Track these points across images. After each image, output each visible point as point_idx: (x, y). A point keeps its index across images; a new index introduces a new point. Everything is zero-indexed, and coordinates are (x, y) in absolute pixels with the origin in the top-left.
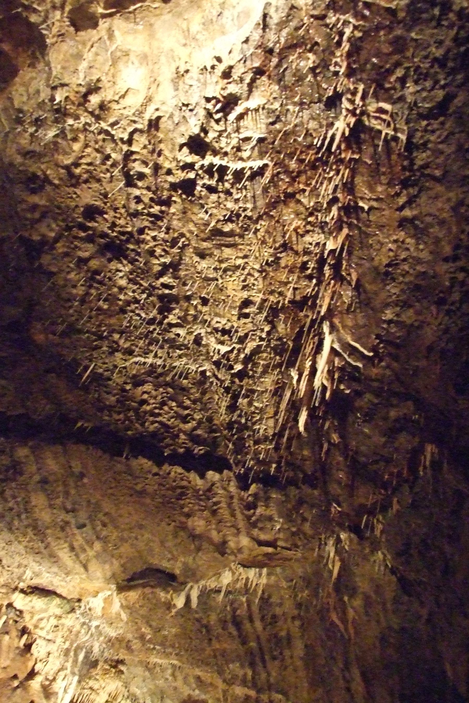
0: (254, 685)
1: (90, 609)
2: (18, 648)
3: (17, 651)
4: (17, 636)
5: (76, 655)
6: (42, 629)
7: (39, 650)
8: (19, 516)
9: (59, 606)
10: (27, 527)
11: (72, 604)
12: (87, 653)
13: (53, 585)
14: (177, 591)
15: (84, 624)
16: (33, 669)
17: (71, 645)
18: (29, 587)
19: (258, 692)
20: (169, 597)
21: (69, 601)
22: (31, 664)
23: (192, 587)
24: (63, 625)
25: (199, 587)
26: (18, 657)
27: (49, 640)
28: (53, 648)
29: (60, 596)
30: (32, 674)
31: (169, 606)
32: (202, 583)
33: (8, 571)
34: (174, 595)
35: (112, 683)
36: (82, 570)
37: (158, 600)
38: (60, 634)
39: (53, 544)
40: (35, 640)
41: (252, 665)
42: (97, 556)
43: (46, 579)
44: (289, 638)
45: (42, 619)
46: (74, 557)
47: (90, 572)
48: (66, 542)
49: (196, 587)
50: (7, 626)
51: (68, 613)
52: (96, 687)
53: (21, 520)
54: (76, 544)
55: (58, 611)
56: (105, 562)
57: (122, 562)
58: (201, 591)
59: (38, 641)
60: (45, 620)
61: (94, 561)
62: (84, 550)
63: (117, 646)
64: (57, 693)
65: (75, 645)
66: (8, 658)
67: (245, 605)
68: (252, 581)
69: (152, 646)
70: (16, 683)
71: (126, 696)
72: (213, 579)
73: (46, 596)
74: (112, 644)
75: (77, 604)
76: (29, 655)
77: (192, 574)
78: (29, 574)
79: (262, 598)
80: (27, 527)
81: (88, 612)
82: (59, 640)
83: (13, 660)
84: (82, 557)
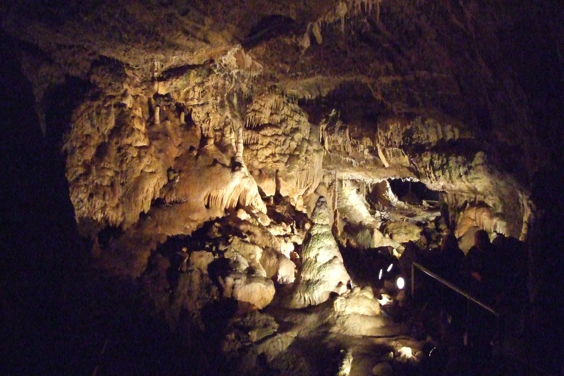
0: (397, 71)
1: (225, 65)
2: (182, 125)
3: (182, 129)
4: (176, 117)
5: (230, 102)
6: (192, 99)
7: (198, 115)
8: (124, 29)
9: (198, 75)
10: (136, 34)
11: (207, 67)
12: (238, 95)
13: (183, 61)
14: (299, 33)
15: (225, 76)
16: (202, 135)
17: (222, 97)
18: (163, 73)
19: (403, 75)
20: (294, 40)
21: (203, 66)
22: (198, 133)
23: (312, 26)
24: (208, 87)
25: (318, 24)
26: (186, 133)
27: (202, 105)
28: (209, 108)
29: (194, 67)
30: (204, 140)
31: (298, 49)
32: (320, 20)
33: (139, 69)
34: (298, 39)
35: (269, 99)
36: (204, 44)
37: (285, 45)
38: (209, 95)
39: (167, 37)
40: (191, 110)
41: (391, 59)
42: (212, 28)
43: (175, 60)
44: (420, 31)
45: (188, 92)
46: (192, 38)
47: (212, 42)
48: (177, 31)
49: (316, 26)
50: (164, 113)
51: (208, 76)
52: (257, 107)
53: (128, 32)
54: (187, 28)
55: (198, 80)
56: (221, 30)
57: (237, 22)
58: (322, 28)
59: (194, 110)
60: (191, 92)
61: (211, 33)
62: (198, 29)
63: (262, 80)
64: (231, 145)
65: (225, 95)
66: (178, 136)
67: (368, 25)
68: (368, 5)
69: (294, 74)
70: (195, 153)
71: (286, 102)
72: (330, 13)
73: (182, 74)
74: (258, 80)
75: (211, 65)
76: (193, 127)
77: (308, 16)
78: (157, 64)
79: (382, 14)
80: (136, 34)
81: (225, 67)
82: (211, 100)
83: (183, 136)
84: (199, 35)
